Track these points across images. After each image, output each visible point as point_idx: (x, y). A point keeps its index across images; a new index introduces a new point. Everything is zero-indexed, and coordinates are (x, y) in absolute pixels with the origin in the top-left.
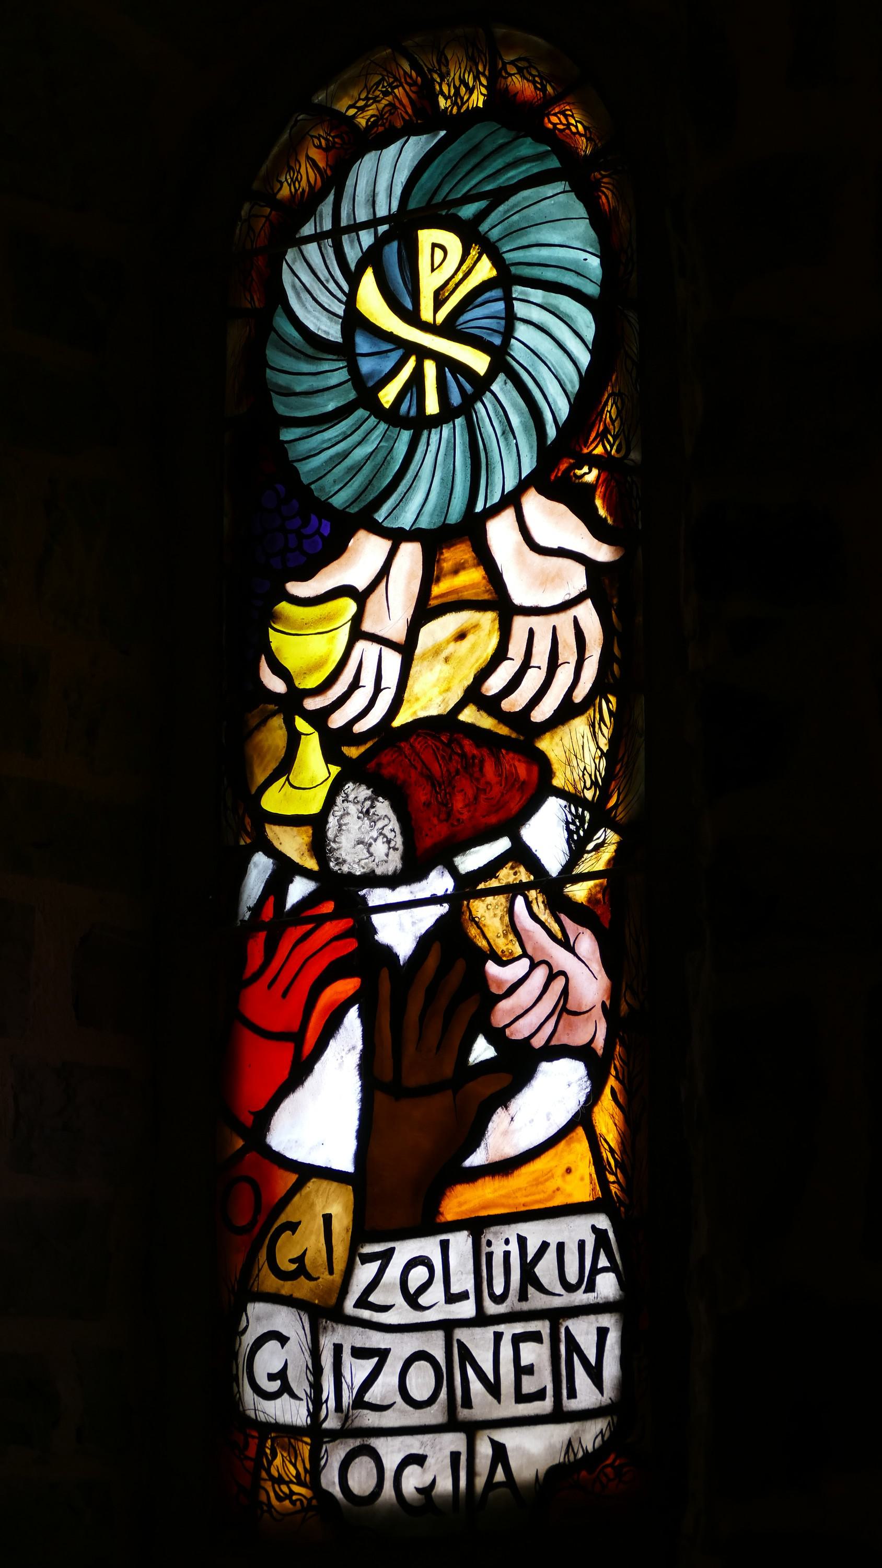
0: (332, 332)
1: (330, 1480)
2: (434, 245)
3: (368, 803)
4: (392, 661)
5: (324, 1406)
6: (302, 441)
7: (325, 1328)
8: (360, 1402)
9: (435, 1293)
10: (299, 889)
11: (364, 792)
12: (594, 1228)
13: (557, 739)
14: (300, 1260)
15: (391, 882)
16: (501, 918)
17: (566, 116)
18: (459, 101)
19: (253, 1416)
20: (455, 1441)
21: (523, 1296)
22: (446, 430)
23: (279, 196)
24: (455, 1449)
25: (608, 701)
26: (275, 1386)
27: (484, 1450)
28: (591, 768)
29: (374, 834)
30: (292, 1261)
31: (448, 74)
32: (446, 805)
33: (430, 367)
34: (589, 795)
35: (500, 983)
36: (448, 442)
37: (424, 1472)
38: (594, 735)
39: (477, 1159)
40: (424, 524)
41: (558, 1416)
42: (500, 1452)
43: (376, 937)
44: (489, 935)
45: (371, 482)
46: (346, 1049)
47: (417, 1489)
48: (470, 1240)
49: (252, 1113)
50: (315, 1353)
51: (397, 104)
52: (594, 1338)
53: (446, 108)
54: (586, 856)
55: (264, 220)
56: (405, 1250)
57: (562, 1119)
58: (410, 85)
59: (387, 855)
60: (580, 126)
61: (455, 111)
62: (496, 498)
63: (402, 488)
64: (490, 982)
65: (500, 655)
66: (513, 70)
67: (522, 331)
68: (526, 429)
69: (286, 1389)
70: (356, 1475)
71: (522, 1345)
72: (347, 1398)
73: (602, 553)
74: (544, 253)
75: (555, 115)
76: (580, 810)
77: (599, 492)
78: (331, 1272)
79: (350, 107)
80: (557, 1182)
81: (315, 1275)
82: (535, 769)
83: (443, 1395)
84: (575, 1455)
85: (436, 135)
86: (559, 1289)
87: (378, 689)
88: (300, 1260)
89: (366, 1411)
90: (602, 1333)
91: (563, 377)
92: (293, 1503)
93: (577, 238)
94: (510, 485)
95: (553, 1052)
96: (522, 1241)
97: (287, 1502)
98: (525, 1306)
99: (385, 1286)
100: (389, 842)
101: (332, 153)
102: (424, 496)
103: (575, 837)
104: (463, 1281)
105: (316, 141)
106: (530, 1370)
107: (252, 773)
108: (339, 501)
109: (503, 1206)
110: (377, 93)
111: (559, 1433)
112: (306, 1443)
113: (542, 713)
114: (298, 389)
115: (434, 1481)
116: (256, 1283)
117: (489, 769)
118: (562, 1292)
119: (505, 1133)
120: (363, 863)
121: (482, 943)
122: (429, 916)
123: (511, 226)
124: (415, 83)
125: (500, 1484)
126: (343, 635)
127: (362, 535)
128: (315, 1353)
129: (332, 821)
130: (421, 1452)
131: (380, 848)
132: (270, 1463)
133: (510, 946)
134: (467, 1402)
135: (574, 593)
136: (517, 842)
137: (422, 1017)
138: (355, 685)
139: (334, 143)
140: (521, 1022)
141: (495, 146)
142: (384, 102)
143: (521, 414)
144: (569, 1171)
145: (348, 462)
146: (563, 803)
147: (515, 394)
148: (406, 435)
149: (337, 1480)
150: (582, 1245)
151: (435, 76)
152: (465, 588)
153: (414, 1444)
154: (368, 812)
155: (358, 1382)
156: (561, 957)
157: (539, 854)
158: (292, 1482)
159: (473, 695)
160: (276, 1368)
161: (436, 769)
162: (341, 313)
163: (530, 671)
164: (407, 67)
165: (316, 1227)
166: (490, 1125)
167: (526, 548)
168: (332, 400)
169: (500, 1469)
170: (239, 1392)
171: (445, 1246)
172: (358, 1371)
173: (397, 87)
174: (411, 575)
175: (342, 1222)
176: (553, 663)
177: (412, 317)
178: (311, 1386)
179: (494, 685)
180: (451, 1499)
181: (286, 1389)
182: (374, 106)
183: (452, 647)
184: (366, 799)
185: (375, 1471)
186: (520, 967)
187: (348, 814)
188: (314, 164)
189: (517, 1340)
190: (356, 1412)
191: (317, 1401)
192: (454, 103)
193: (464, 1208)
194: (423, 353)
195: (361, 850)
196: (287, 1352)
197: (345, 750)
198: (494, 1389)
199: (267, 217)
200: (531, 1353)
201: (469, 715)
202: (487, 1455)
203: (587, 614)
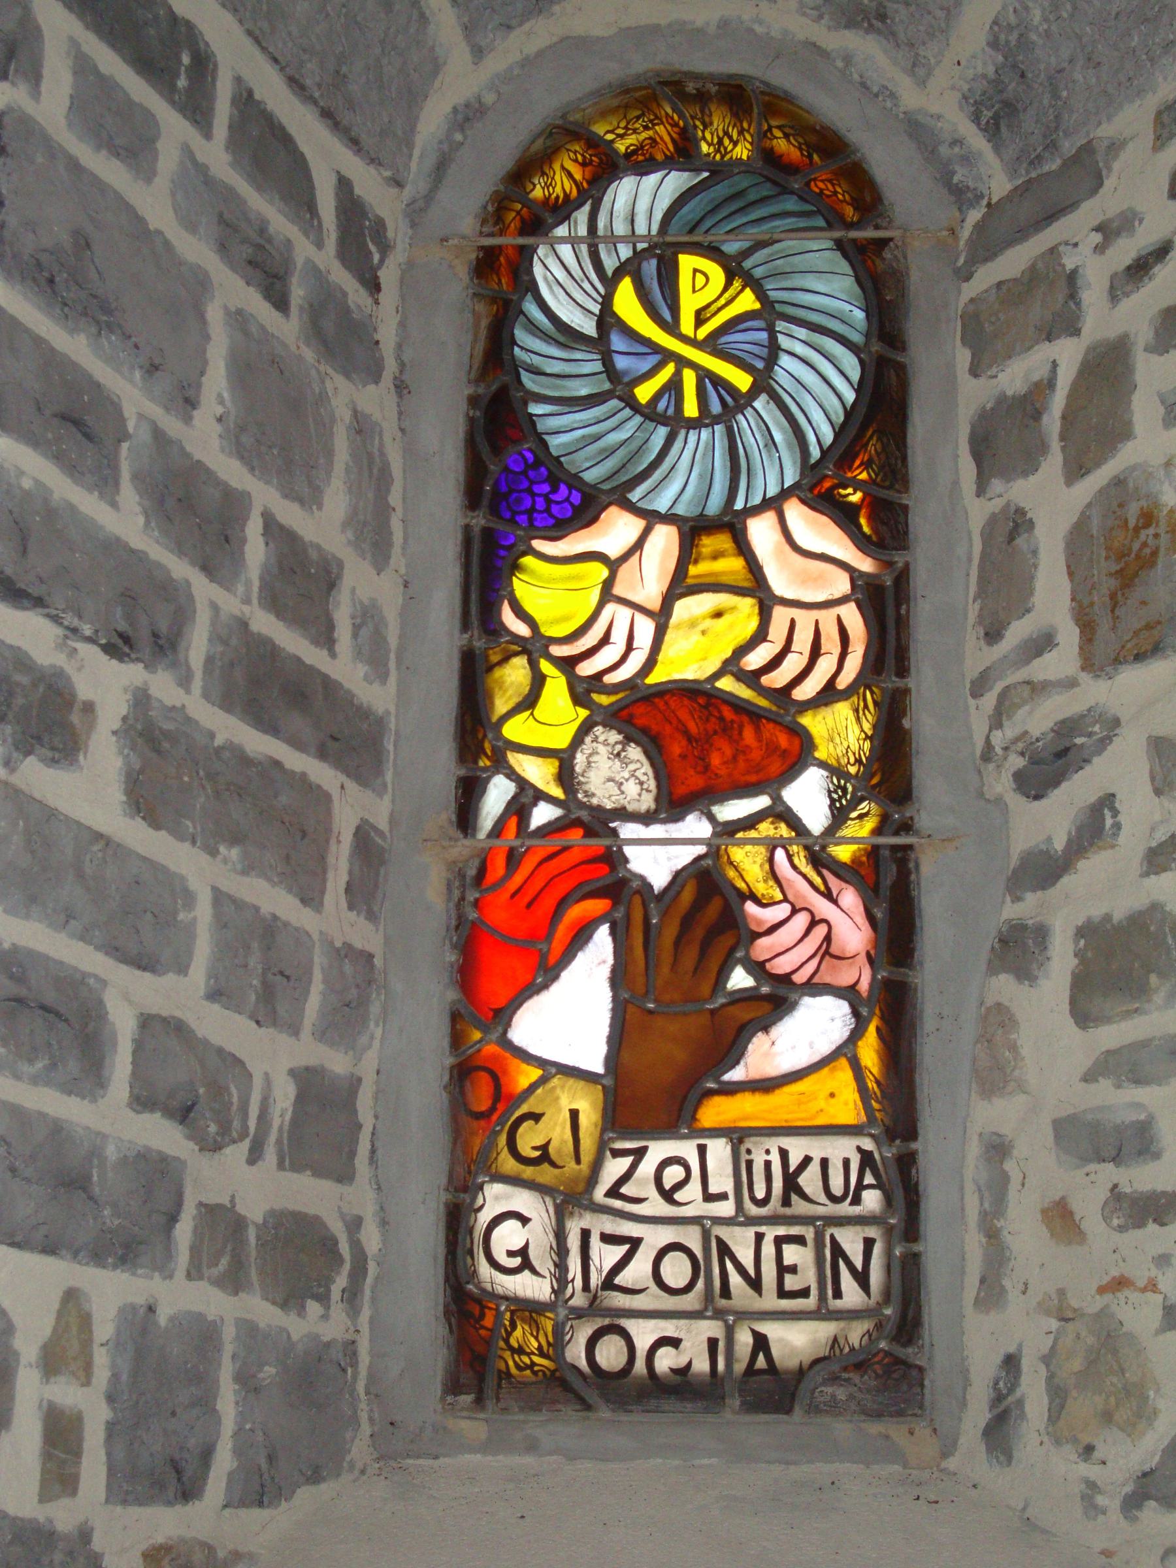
0: (586, 326)
1: (576, 1353)
2: (695, 271)
3: (619, 747)
4: (645, 629)
5: (570, 1285)
6: (551, 418)
7: (572, 1213)
8: (609, 1283)
9: (692, 1191)
10: (542, 815)
11: (614, 737)
12: (859, 1149)
13: (819, 717)
14: (544, 1148)
15: (646, 818)
16: (761, 866)
17: (833, 185)
18: (722, 149)
19: (490, 1289)
20: (711, 1328)
21: (786, 1202)
22: (705, 434)
23: (531, 196)
24: (712, 1335)
25: (872, 693)
26: (516, 1262)
27: (744, 1339)
28: (855, 747)
29: (626, 775)
30: (535, 1148)
31: (711, 124)
32: (703, 760)
33: (689, 379)
34: (853, 770)
35: (759, 922)
36: (707, 444)
37: (678, 1355)
38: (858, 719)
39: (736, 1074)
40: (680, 510)
41: (821, 1314)
42: (761, 1342)
43: (629, 866)
44: (748, 879)
45: (624, 466)
46: (597, 962)
47: (672, 1370)
48: (729, 1148)
49: (491, 1009)
50: (560, 1235)
51: (658, 139)
52: (860, 1247)
53: (708, 155)
54: (849, 822)
55: (513, 214)
56: (658, 1150)
57: (825, 1048)
58: (672, 126)
59: (640, 795)
60: (847, 196)
61: (718, 157)
62: (757, 500)
63: (658, 475)
64: (749, 920)
65: (760, 636)
66: (777, 133)
67: (785, 360)
68: (789, 446)
69: (527, 1265)
70: (605, 1353)
71: (784, 1246)
72: (595, 1280)
73: (865, 565)
74: (807, 299)
75: (822, 181)
76: (842, 782)
77: (863, 511)
78: (578, 1161)
79: (608, 132)
80: (821, 1103)
81: (559, 1163)
82: (797, 742)
83: (700, 1284)
84: (841, 1350)
85: (698, 175)
86: (823, 1198)
87: (630, 648)
88: (544, 1148)
89: (615, 1293)
90: (869, 1243)
91: (828, 407)
92: (535, 1373)
93: (842, 292)
94: (772, 491)
95: (814, 988)
96: (784, 1154)
97: (528, 1372)
98: (788, 1211)
99: (637, 1180)
100: (641, 783)
101: (588, 169)
102: (681, 486)
103: (838, 805)
104: (721, 1181)
105: (572, 155)
106: (793, 1269)
107: (492, 703)
108: (590, 476)
109: (764, 1119)
110: (637, 125)
111: (824, 1331)
112: (549, 1318)
113: (807, 690)
114: (549, 371)
115: (690, 1363)
116: (494, 1166)
117: (748, 735)
118: (827, 1202)
119: (767, 1055)
120: (613, 798)
121: (741, 885)
122: (685, 856)
123: (776, 268)
124: (675, 125)
125: (761, 1372)
126: (595, 595)
127: (613, 511)
128: (560, 1235)
129: (580, 759)
130: (675, 1335)
131: (632, 788)
132: (509, 1334)
133: (770, 891)
134: (726, 1292)
135: (837, 595)
136: (777, 799)
137: (677, 944)
138: (605, 640)
139: (591, 161)
140: (781, 958)
141: (758, 197)
142: (645, 135)
143: (782, 429)
144: (832, 1095)
145: (601, 444)
146: (825, 774)
147: (778, 413)
148: (662, 432)
149: (583, 1355)
150: (846, 1163)
151: (698, 123)
152: (723, 573)
153: (669, 1328)
154: (618, 755)
155: (607, 1266)
156: (823, 907)
157: (800, 815)
158: (533, 1354)
159: (731, 665)
160: (517, 1245)
161: (693, 727)
162: (597, 312)
163: (790, 656)
164: (669, 111)
165: (561, 1118)
166: (750, 1047)
167: (787, 548)
168: (585, 386)
169: (761, 1357)
170: (473, 1264)
171: (702, 1150)
172: (611, 1255)
173: (658, 124)
174: (666, 552)
175: (589, 1118)
176: (816, 652)
177: (672, 327)
178: (556, 1265)
179: (755, 660)
180: (708, 1379)
181: (527, 1265)
182: (634, 136)
183: (709, 623)
184: (617, 743)
185: (625, 1349)
186: (780, 912)
187: (597, 753)
188: (570, 175)
189: (779, 1241)
190: (606, 1293)
191: (561, 1279)
192: (718, 151)
193: (722, 1118)
194: (683, 362)
195: (612, 788)
196: (529, 1231)
197: (595, 696)
198: (755, 1283)
199: (518, 213)
200: (791, 1253)
201: (726, 684)
202: (747, 1345)
203: (852, 616)
